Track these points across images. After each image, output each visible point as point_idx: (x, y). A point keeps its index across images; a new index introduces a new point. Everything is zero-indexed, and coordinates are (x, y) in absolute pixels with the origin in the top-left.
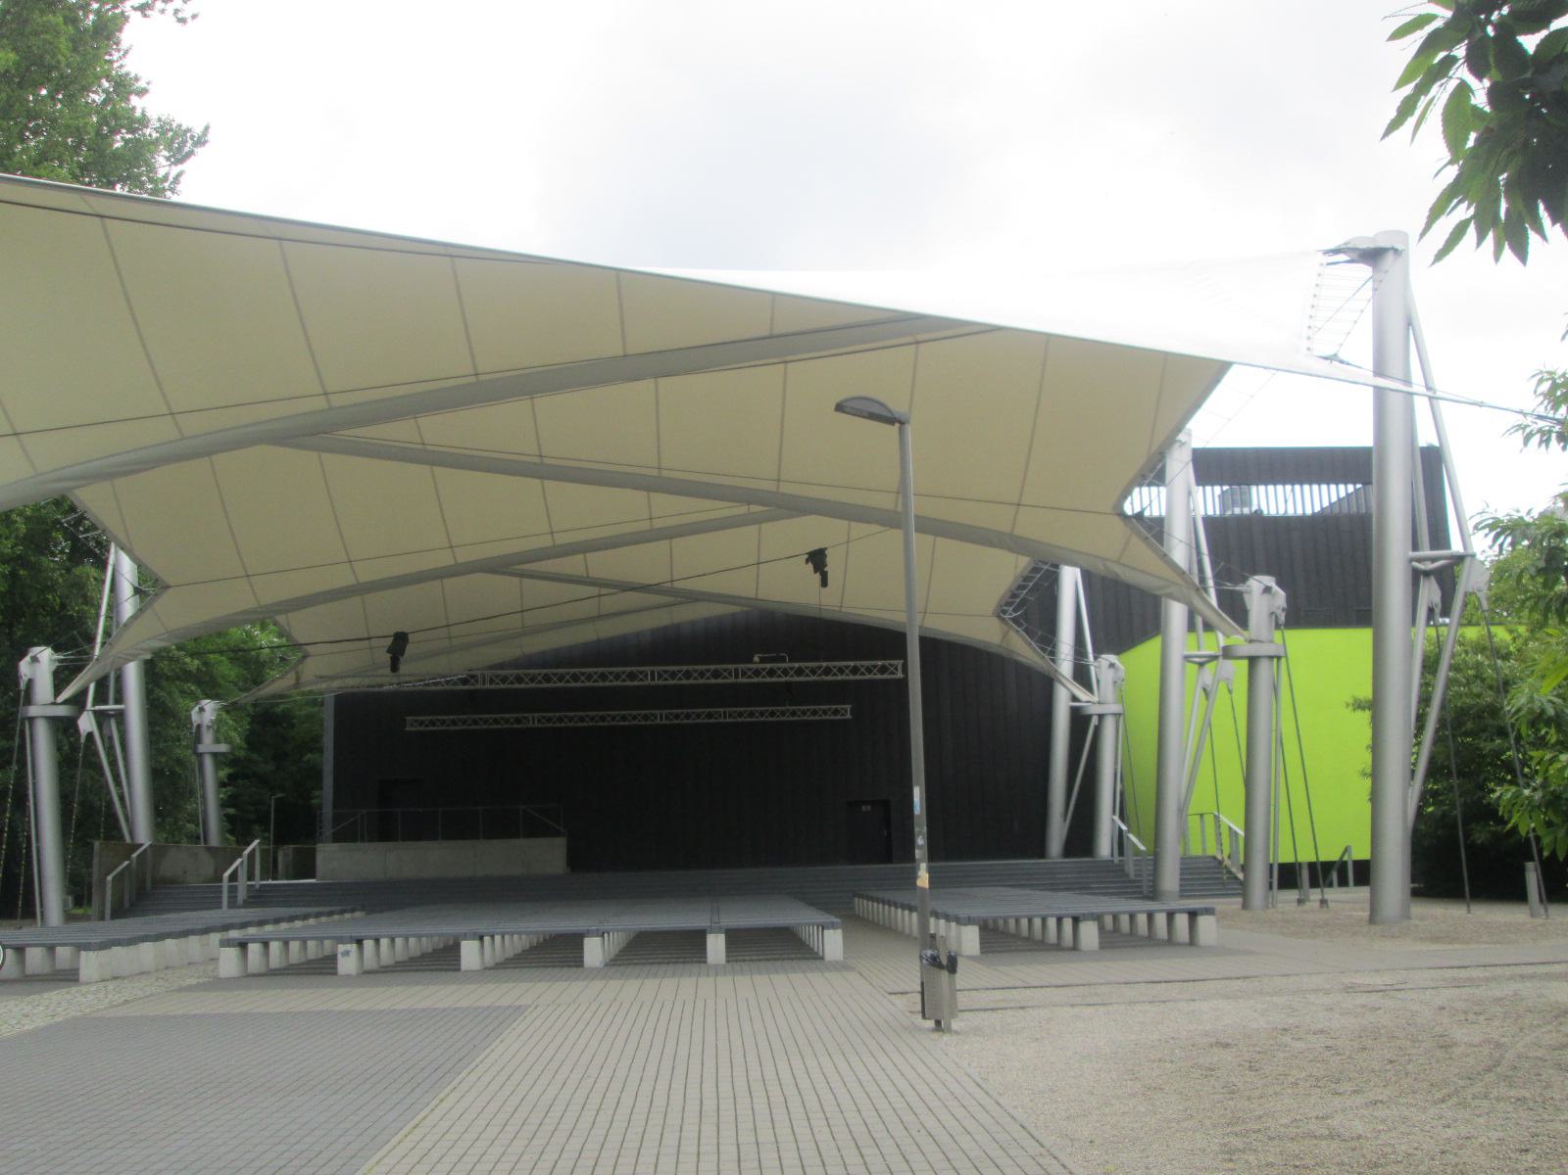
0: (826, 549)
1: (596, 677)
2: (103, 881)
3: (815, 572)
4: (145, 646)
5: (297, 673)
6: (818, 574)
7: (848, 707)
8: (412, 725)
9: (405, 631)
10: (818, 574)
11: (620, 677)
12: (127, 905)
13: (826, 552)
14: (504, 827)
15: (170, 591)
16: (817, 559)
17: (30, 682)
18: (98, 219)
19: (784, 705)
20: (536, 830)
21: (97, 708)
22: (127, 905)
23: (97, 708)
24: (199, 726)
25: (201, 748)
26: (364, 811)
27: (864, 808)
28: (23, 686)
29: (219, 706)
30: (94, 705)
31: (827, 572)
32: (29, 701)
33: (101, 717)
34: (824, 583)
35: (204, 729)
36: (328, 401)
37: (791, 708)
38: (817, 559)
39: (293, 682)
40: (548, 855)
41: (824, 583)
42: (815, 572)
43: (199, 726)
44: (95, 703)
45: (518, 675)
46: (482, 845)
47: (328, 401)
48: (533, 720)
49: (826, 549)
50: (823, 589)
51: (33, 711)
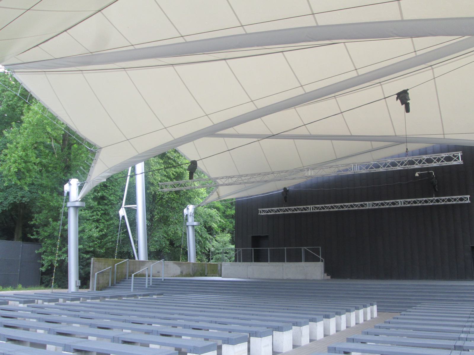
0: (408, 90)
1: (423, 201)
2: (94, 274)
3: (402, 104)
4: (103, 175)
5: (217, 192)
6: (404, 106)
7: (468, 196)
8: (263, 212)
9: (196, 160)
10: (404, 106)
11: (433, 201)
12: (115, 283)
13: (408, 91)
14: (295, 257)
15: (103, 149)
16: (403, 97)
17: (68, 193)
18: (281, 53)
19: (432, 197)
20: (310, 258)
21: (126, 206)
22: (115, 283)
23: (126, 206)
24: (187, 215)
25: (188, 224)
26: (241, 249)
27: (39, 331)
28: (65, 194)
29: (194, 207)
30: (125, 205)
31: (409, 103)
32: (67, 200)
33: (128, 211)
34: (407, 110)
35: (189, 216)
36: (444, 136)
37: (436, 198)
38: (403, 97)
39: (217, 196)
40: (315, 270)
41: (407, 110)
42: (402, 104)
43: (187, 215)
44: (126, 204)
45: (392, 202)
46: (286, 265)
47: (444, 136)
48: (311, 209)
49: (408, 90)
50: (407, 114)
51: (69, 204)
